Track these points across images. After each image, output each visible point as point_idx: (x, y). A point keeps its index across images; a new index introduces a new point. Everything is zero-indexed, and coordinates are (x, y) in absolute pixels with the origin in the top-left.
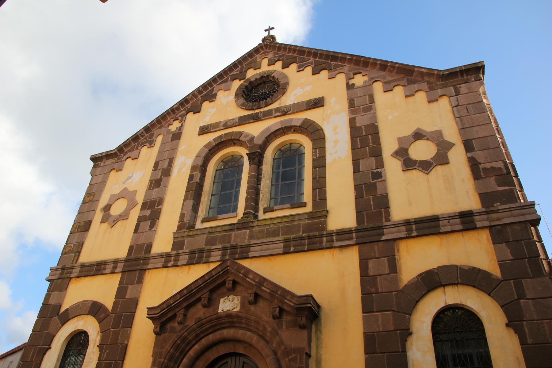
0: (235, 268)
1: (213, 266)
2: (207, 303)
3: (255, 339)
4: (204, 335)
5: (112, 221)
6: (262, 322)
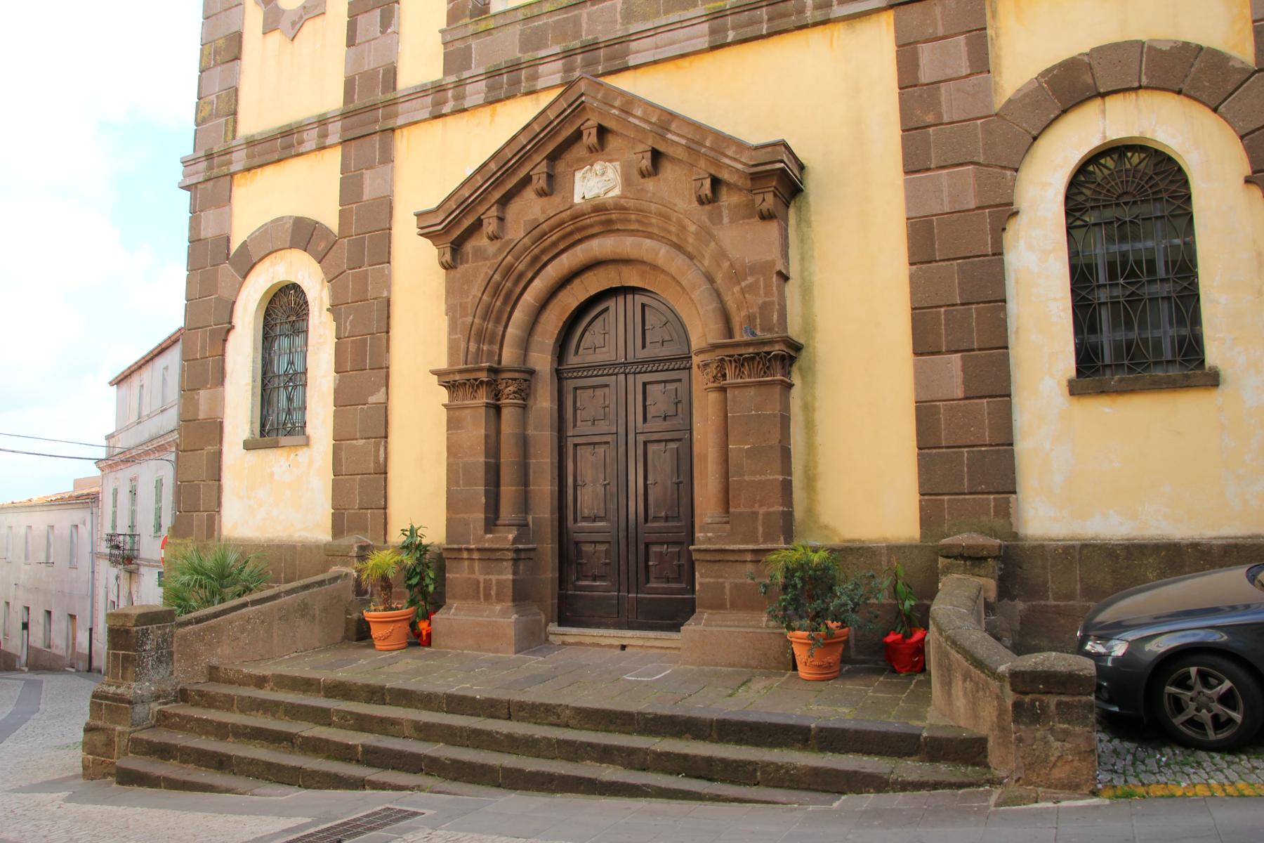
0: (599, 97)
1: (546, 99)
2: (545, 186)
3: (660, 253)
4: (548, 257)
5: (290, 25)
6: (675, 214)
